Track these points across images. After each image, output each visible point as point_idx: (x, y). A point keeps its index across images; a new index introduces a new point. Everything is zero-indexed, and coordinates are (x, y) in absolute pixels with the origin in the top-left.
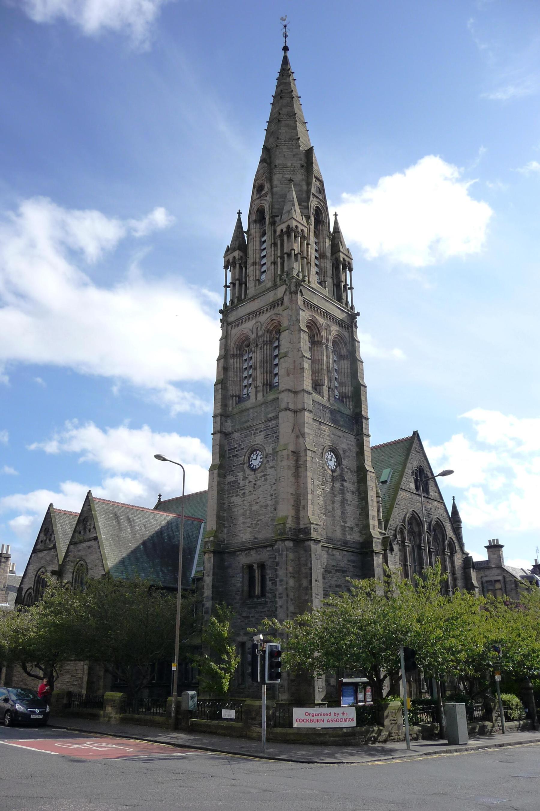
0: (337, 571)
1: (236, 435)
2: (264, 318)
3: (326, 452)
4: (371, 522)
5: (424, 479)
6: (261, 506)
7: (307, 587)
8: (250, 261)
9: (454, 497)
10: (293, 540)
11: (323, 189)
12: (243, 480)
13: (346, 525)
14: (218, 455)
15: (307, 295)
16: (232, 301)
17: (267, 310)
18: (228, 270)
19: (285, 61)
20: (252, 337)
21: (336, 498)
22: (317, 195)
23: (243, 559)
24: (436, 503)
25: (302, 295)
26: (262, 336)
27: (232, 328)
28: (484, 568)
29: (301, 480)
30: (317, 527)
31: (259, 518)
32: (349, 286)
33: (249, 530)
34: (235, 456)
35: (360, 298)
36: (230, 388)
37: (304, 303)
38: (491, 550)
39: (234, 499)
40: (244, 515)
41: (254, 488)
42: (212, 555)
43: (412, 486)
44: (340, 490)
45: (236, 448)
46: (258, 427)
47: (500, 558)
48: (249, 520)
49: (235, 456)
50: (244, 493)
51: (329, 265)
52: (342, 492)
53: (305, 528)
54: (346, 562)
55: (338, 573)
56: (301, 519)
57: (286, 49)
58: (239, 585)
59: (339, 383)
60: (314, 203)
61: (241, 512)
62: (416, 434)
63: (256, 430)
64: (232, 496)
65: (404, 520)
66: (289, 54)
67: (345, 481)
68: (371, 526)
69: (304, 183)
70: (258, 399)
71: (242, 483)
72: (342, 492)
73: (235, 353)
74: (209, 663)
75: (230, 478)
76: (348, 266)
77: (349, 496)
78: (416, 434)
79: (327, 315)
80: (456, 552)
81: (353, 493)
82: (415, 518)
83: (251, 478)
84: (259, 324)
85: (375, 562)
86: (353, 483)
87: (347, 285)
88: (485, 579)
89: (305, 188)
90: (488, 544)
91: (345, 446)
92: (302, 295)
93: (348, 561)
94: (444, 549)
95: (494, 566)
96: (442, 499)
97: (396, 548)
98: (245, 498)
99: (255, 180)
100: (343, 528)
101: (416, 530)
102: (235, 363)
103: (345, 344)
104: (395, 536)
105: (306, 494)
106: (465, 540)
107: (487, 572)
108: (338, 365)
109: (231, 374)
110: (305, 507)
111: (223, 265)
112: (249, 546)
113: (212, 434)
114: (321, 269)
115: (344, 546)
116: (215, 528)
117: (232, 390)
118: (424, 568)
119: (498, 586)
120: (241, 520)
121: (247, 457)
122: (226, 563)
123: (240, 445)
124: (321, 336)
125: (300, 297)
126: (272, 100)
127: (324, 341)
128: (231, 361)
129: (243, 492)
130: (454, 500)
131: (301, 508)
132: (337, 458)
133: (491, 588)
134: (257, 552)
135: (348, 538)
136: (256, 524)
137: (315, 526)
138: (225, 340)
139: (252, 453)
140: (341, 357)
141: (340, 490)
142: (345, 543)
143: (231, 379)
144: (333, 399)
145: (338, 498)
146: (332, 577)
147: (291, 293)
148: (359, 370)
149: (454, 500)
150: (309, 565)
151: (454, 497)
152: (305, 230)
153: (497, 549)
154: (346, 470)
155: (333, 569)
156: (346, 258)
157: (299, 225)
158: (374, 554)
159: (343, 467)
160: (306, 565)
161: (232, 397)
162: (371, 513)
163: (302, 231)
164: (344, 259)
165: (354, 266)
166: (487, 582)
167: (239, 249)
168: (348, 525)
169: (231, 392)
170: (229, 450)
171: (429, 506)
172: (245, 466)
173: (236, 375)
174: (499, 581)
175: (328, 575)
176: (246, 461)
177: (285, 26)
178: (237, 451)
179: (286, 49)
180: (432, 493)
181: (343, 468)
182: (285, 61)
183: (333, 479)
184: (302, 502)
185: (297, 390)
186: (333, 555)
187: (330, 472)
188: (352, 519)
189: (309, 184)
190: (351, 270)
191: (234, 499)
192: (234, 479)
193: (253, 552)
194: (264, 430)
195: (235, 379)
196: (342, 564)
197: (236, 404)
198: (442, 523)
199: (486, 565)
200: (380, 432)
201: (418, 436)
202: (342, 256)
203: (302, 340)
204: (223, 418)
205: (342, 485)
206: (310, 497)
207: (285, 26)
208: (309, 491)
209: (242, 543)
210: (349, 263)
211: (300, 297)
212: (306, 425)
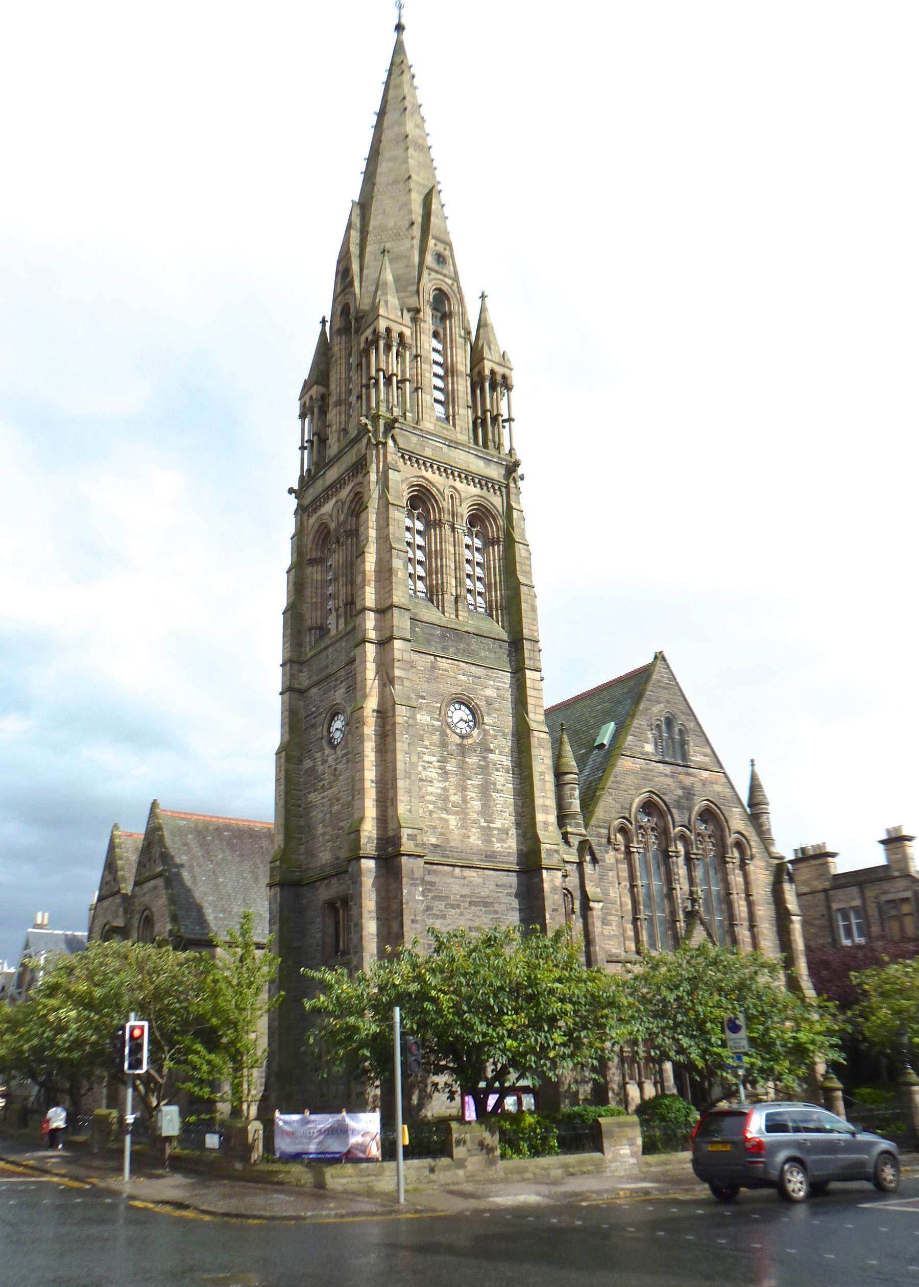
0: (471, 903)
3: (447, 705)
4: (540, 817)
5: (679, 736)
6: (343, 805)
7: (398, 934)
8: (332, 400)
9: (752, 761)
12: (322, 764)
13: (491, 825)
14: (287, 728)
16: (309, 470)
17: (349, 479)
18: (307, 421)
19: (399, 48)
21: (469, 782)
26: (345, 522)
27: (308, 516)
28: (881, 880)
29: (389, 757)
30: (415, 832)
31: (341, 824)
32: (506, 417)
35: (523, 437)
36: (308, 615)
38: (890, 846)
39: (312, 797)
40: (323, 821)
41: (335, 775)
42: (278, 889)
45: (313, 713)
46: (338, 675)
47: (905, 859)
48: (328, 829)
50: (324, 785)
53: (394, 836)
54: (492, 887)
55: (473, 908)
56: (389, 821)
57: (399, 28)
58: (319, 935)
61: (320, 815)
62: (659, 657)
63: (336, 680)
64: (309, 793)
66: (406, 36)
67: (492, 751)
70: (340, 628)
71: (320, 769)
73: (314, 556)
74: (904, 1062)
75: (308, 764)
76: (501, 383)
78: (659, 657)
79: (448, 470)
80: (752, 858)
84: (340, 503)
85: (546, 885)
88: (884, 898)
90: (884, 837)
91: (490, 692)
95: (896, 874)
96: (721, 767)
97: (610, 857)
98: (325, 794)
102: (314, 573)
105: (394, 780)
107: (886, 886)
109: (308, 592)
110: (394, 801)
111: (297, 412)
112: (329, 871)
113: (281, 694)
115: (488, 861)
116: (282, 846)
117: (311, 617)
118: (675, 889)
119: (906, 908)
120: (320, 829)
121: (326, 726)
122: (304, 901)
123: (318, 708)
127: (446, 517)
128: (309, 570)
129: (321, 784)
130: (753, 765)
131: (389, 804)
133: (893, 913)
134: (338, 880)
135: (497, 846)
137: (410, 831)
139: (332, 719)
140: (489, 542)
143: (309, 600)
144: (466, 614)
146: (461, 914)
148: (518, 559)
149: (753, 765)
150: (399, 897)
151: (752, 761)
153: (898, 844)
154: (492, 732)
155: (463, 901)
158: (544, 872)
159: (487, 727)
160: (396, 897)
161: (311, 629)
162: (538, 802)
166: (888, 902)
168: (498, 824)
169: (308, 623)
170: (306, 717)
171: (688, 781)
172: (324, 741)
173: (316, 593)
174: (906, 900)
175: (453, 912)
176: (325, 733)
178: (315, 718)
179: (399, 28)
181: (484, 730)
182: (399, 48)
183: (463, 750)
184: (391, 795)
185: (384, 607)
186: (464, 878)
187: (458, 740)
190: (509, 388)
191: (312, 797)
192: (311, 764)
193: (334, 881)
194: (345, 680)
195: (314, 600)
196: (485, 892)
197: (316, 641)
198: (719, 809)
199: (883, 875)
201: (664, 659)
203: (391, 522)
204: (296, 667)
206: (401, 784)
209: (323, 867)
210: (504, 377)
212: (396, 664)
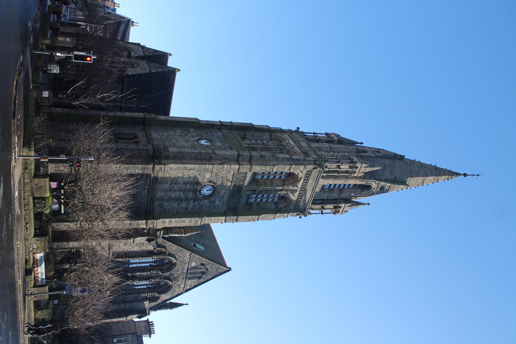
1: (220, 134)
2: (296, 148)
4: (167, 220)
5: (200, 277)
8: (332, 145)
10: (153, 154)
11: (383, 193)
15: (315, 173)
19: (458, 174)
20: (284, 144)
22: (379, 187)
23: (140, 135)
24: (183, 286)
25: (314, 169)
30: (163, 171)
33: (159, 137)
34: (206, 133)
37: (309, 171)
40: (169, 135)
43: (193, 264)
44: (188, 198)
48: (165, 137)
49: (206, 133)
51: (335, 195)
52: (187, 199)
57: (465, 175)
59: (259, 202)
60: (374, 184)
62: (229, 269)
65: (170, 255)
67: (194, 203)
68: (164, 220)
69: (385, 178)
71: (190, 135)
72: (187, 199)
77: (184, 205)
78: (229, 269)
81: (186, 208)
82: (172, 266)
83: (192, 139)
85: (140, 221)
86: (192, 209)
87: (324, 209)
89: (383, 178)
91: (217, 203)
92: (314, 169)
93: (141, 202)
94: (152, 292)
99: (383, 150)
100: (162, 199)
101: (164, 268)
103: (285, 207)
104: (159, 246)
105: (184, 163)
106: (159, 312)
108: (271, 201)
111: (328, 132)
114: (332, 190)
124: (288, 186)
125: (312, 167)
126: (433, 164)
132: (209, 195)
135: (156, 203)
136: (163, 141)
137: (163, 169)
138: (281, 131)
141: (188, 198)
142: (152, 200)
145: (182, 195)
147: (314, 161)
152: (356, 175)
156: (341, 209)
157: (358, 169)
162: (174, 220)
163: (355, 172)
164: (340, 207)
165: (338, 215)
167: (339, 140)
168: (165, 204)
177: (478, 175)
179: (465, 175)
180: (190, 282)
182: (458, 174)
188: (169, 207)
189: (386, 181)
190: (334, 213)
197: (240, 136)
200: (229, 234)
201: (228, 271)
202: (343, 205)
205: (191, 199)
206: (182, 166)
207: (478, 175)
208: (186, 166)
209: (151, 134)
210: (339, 211)
211: (312, 167)
